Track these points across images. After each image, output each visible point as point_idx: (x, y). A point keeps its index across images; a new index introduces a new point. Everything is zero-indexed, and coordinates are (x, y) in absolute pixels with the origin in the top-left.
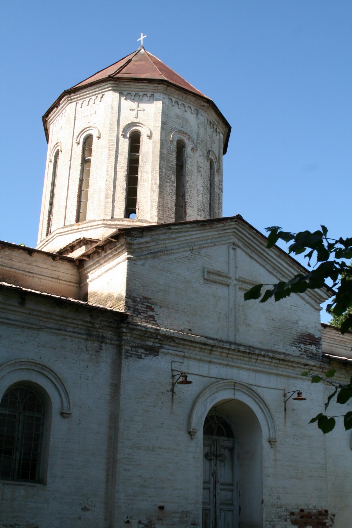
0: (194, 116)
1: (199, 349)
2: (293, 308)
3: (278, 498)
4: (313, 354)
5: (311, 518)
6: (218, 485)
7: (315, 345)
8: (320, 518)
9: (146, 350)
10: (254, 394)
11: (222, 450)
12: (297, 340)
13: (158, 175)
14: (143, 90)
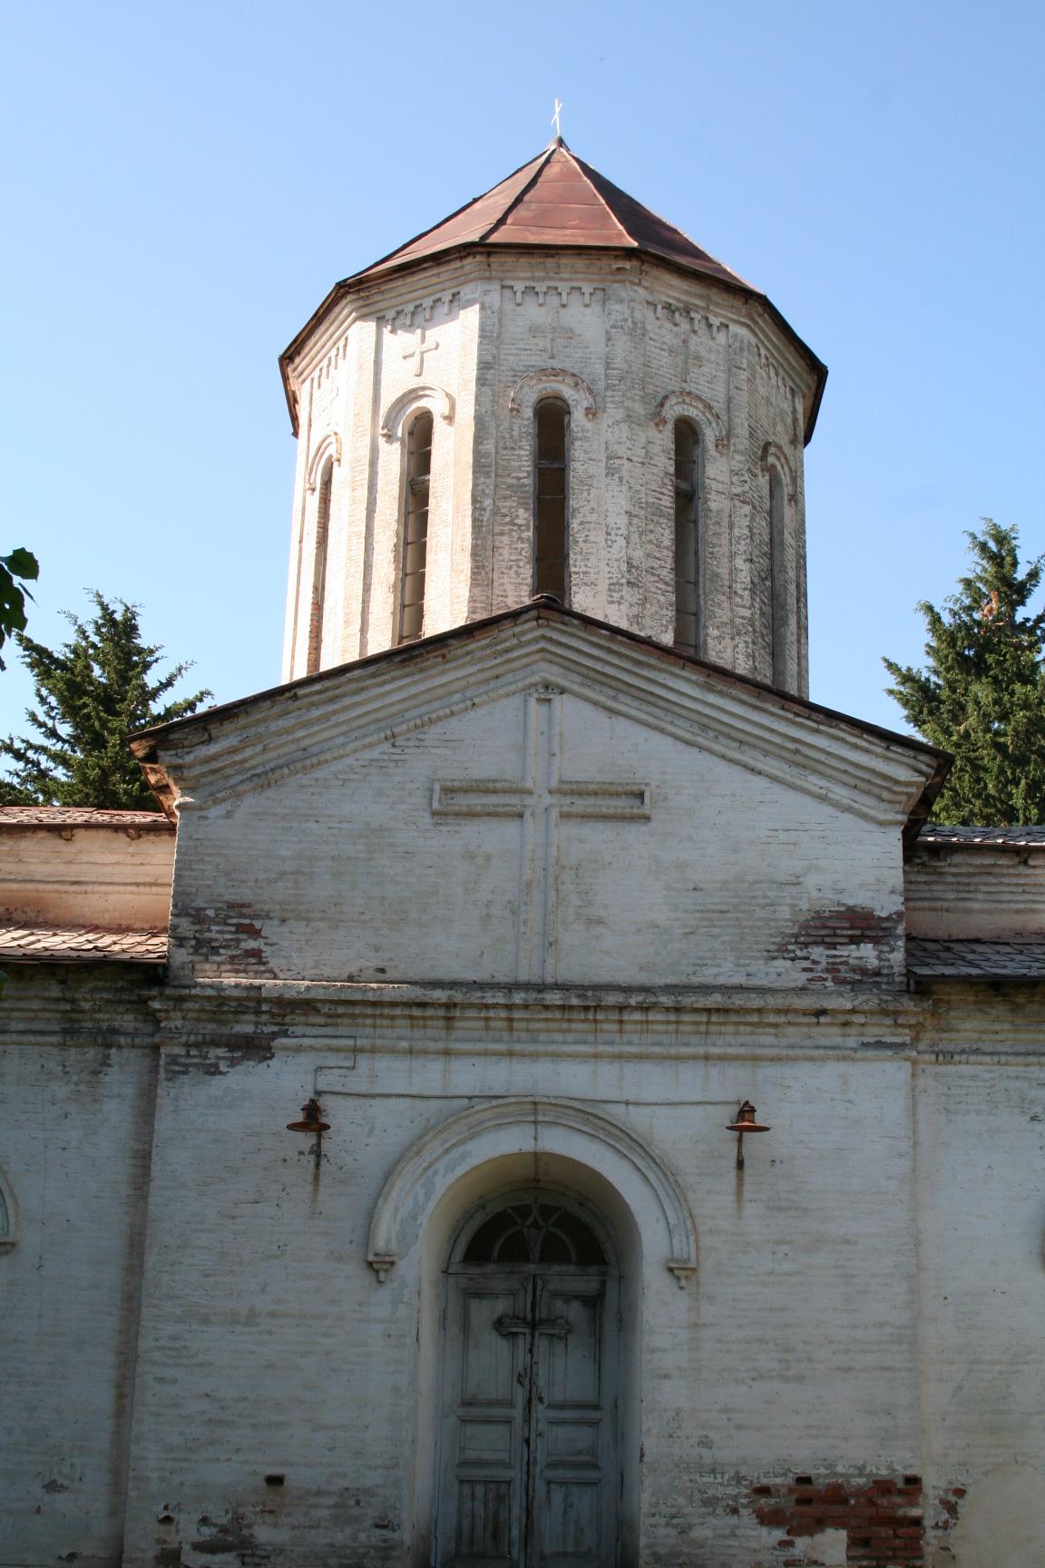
0: (596, 308)
1: (407, 1022)
2: (782, 836)
3: (705, 1443)
4: (863, 971)
5: (845, 1501)
6: (540, 1411)
7: (876, 941)
8: (884, 1501)
9: (232, 1048)
10: (609, 1127)
11: (559, 1303)
12: (796, 936)
13: (469, 521)
14: (431, 290)
